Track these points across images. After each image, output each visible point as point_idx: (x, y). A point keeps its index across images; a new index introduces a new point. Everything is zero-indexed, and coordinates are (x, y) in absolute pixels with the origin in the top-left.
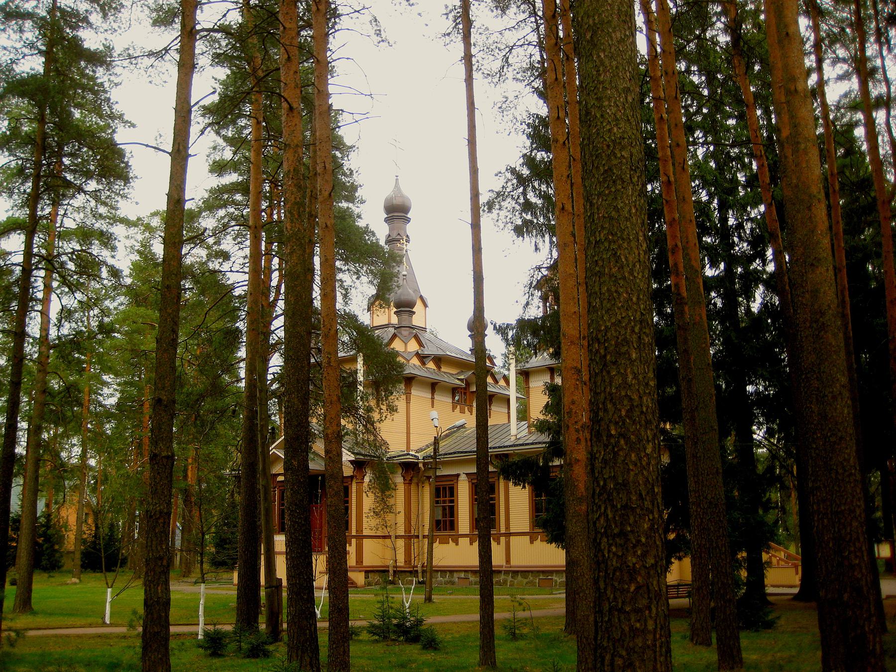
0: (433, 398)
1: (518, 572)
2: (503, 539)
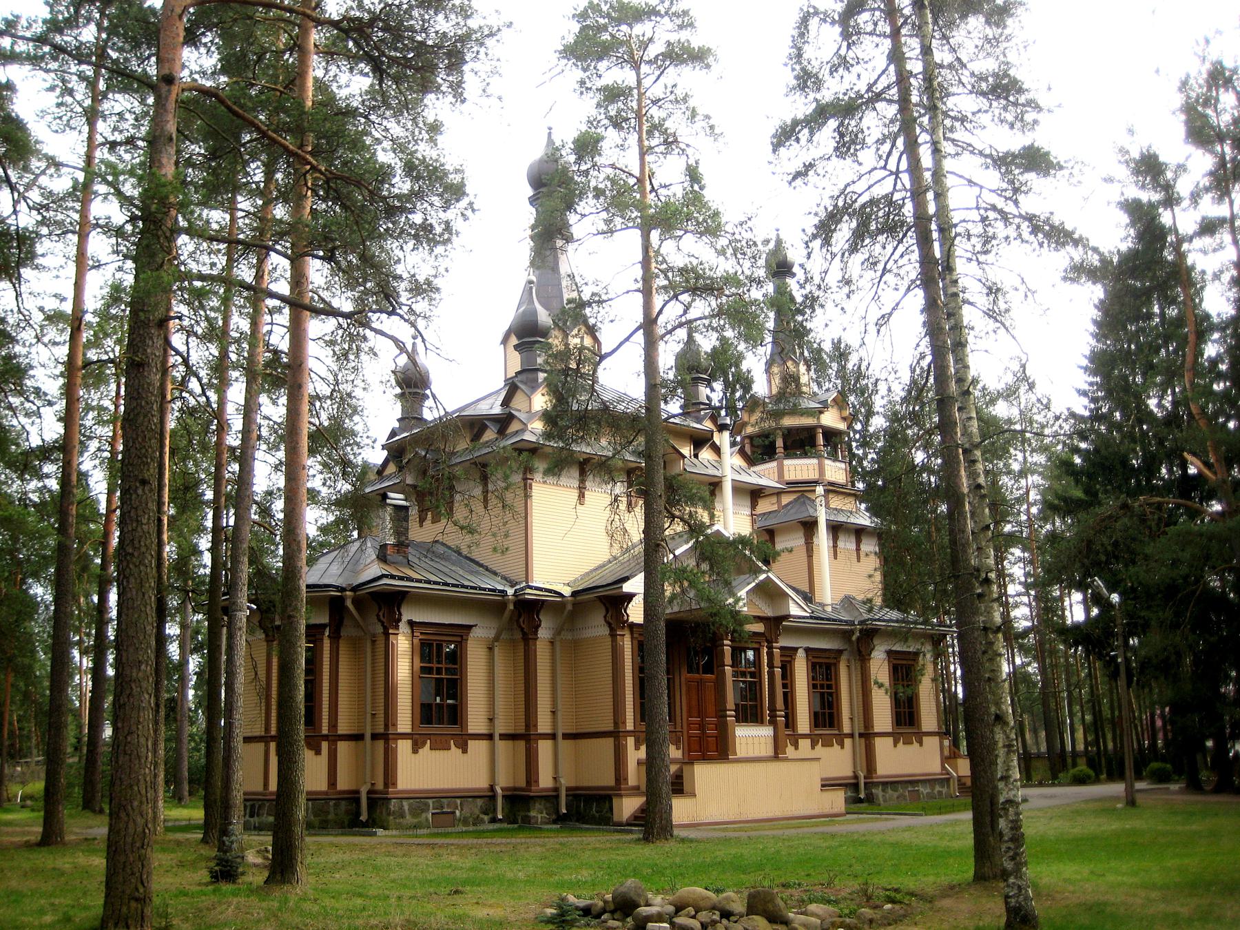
0: (858, 549)
1: (887, 783)
2: (325, 745)
